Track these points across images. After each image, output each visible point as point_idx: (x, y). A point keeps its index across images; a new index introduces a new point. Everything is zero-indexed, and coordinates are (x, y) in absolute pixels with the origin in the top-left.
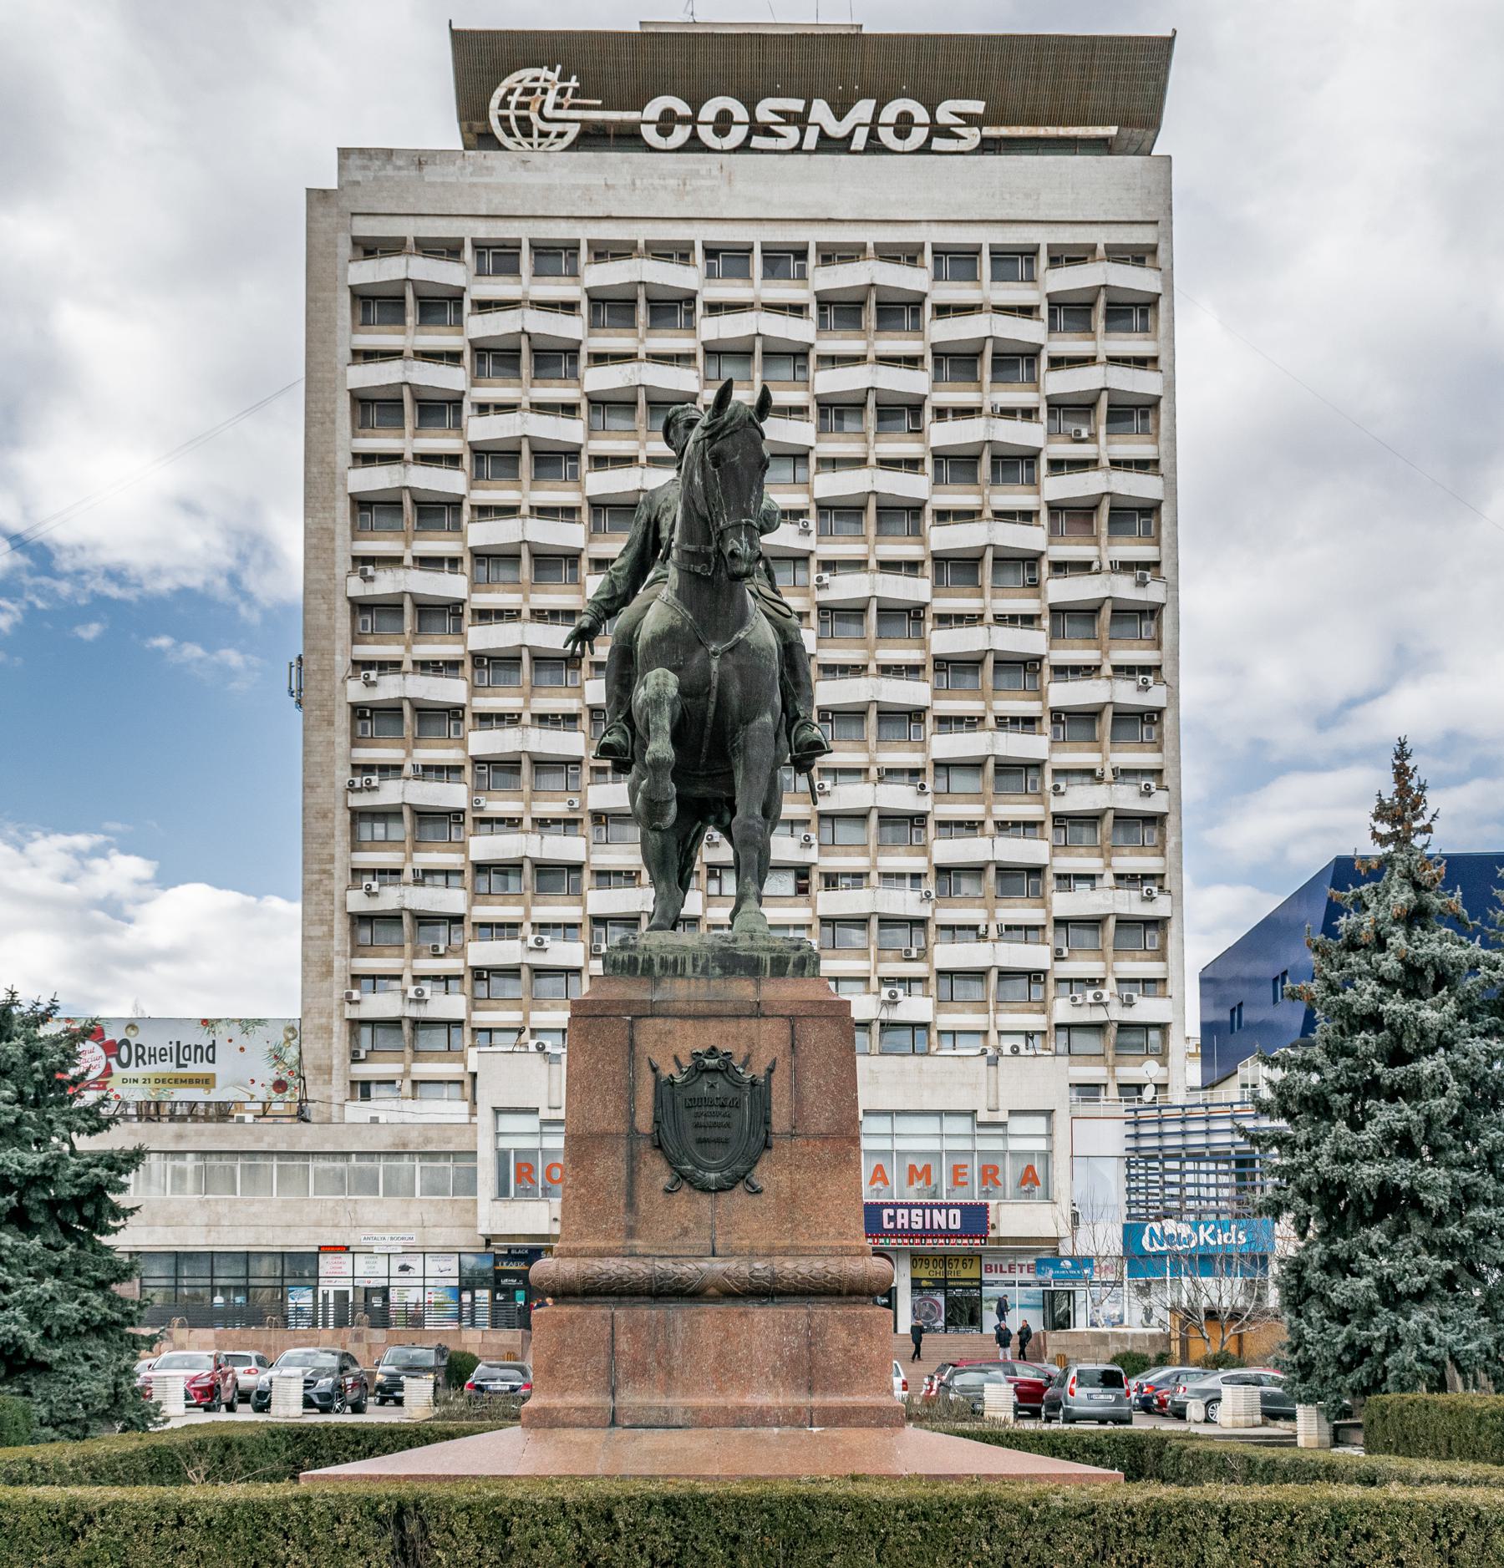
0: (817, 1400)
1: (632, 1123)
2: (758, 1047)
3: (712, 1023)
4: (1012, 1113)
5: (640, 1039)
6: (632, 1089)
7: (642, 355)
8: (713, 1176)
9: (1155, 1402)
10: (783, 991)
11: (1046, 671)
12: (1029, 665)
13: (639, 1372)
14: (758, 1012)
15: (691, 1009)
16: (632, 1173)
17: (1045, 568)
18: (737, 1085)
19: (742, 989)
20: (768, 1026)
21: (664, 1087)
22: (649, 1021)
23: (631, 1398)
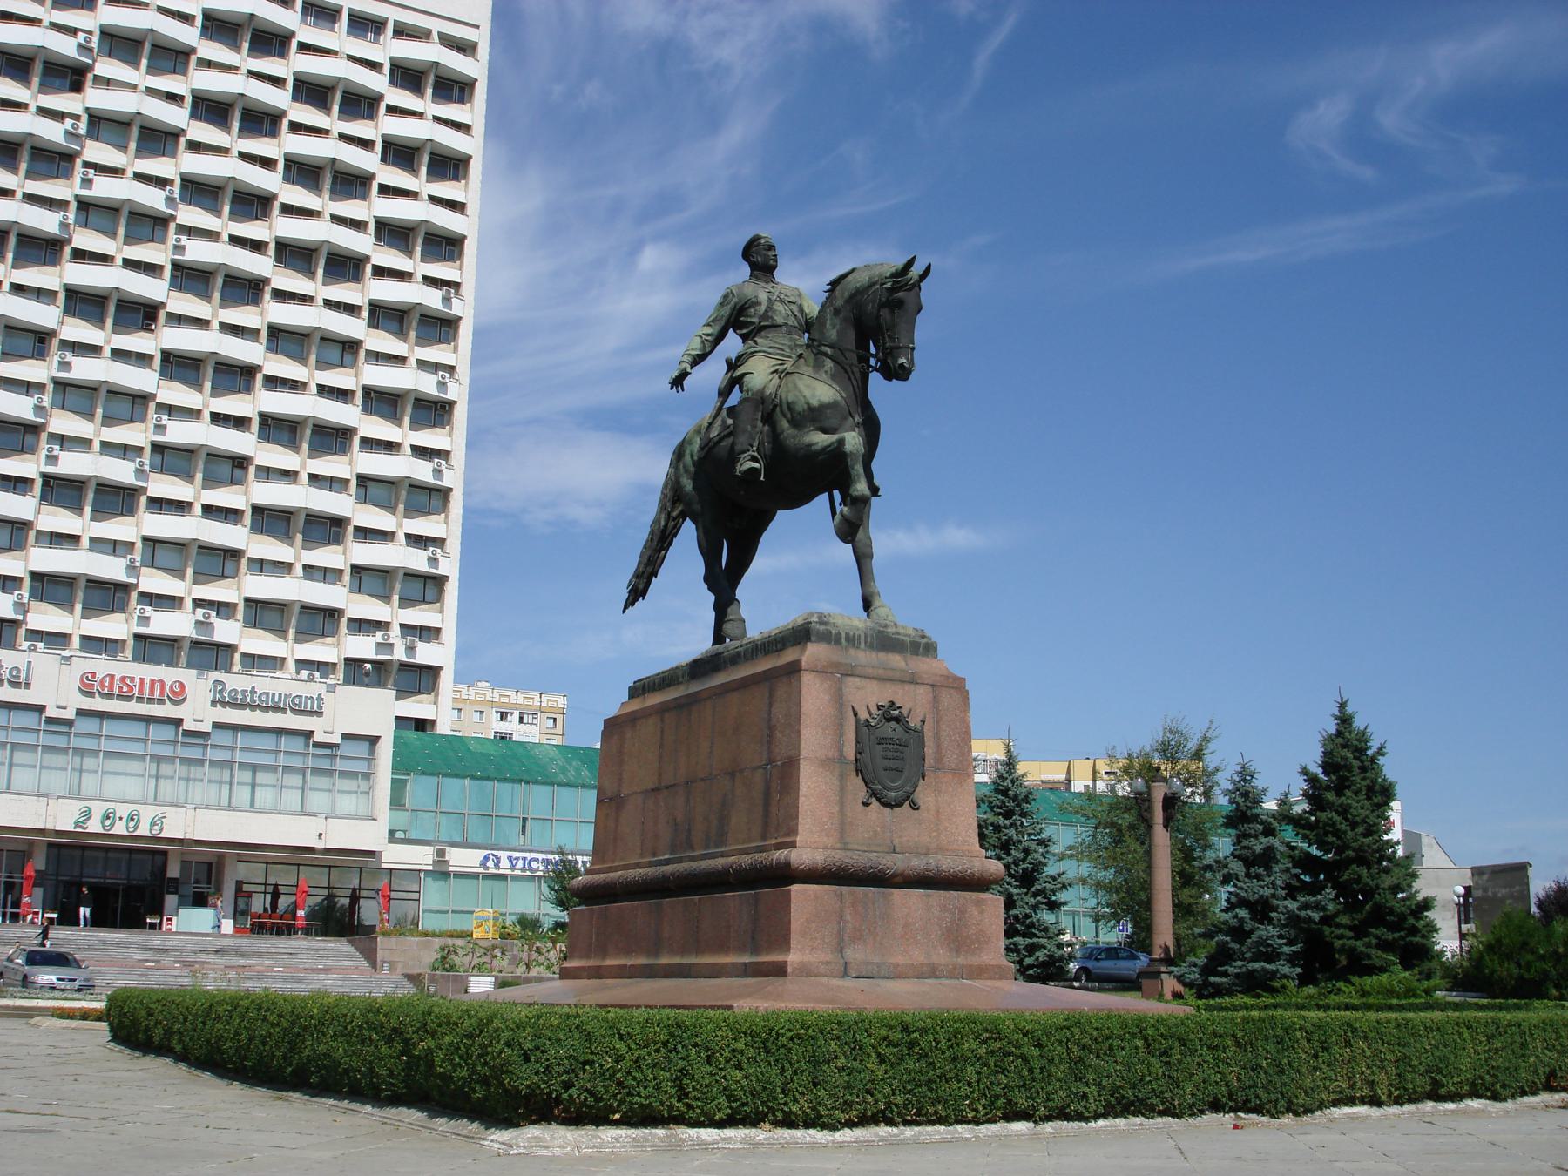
0: (961, 960)
1: (841, 751)
2: (914, 703)
3: (888, 685)
4: (345, 737)
5: (846, 690)
6: (841, 726)
7: (46, 23)
8: (893, 794)
9: (143, 1013)
10: (922, 665)
11: (362, 353)
12: (350, 347)
13: (858, 937)
14: (913, 680)
15: (875, 673)
16: (842, 789)
17: (369, 269)
18: (907, 729)
19: (896, 660)
20: (921, 690)
21: (863, 727)
22: (851, 679)
23: (855, 954)
